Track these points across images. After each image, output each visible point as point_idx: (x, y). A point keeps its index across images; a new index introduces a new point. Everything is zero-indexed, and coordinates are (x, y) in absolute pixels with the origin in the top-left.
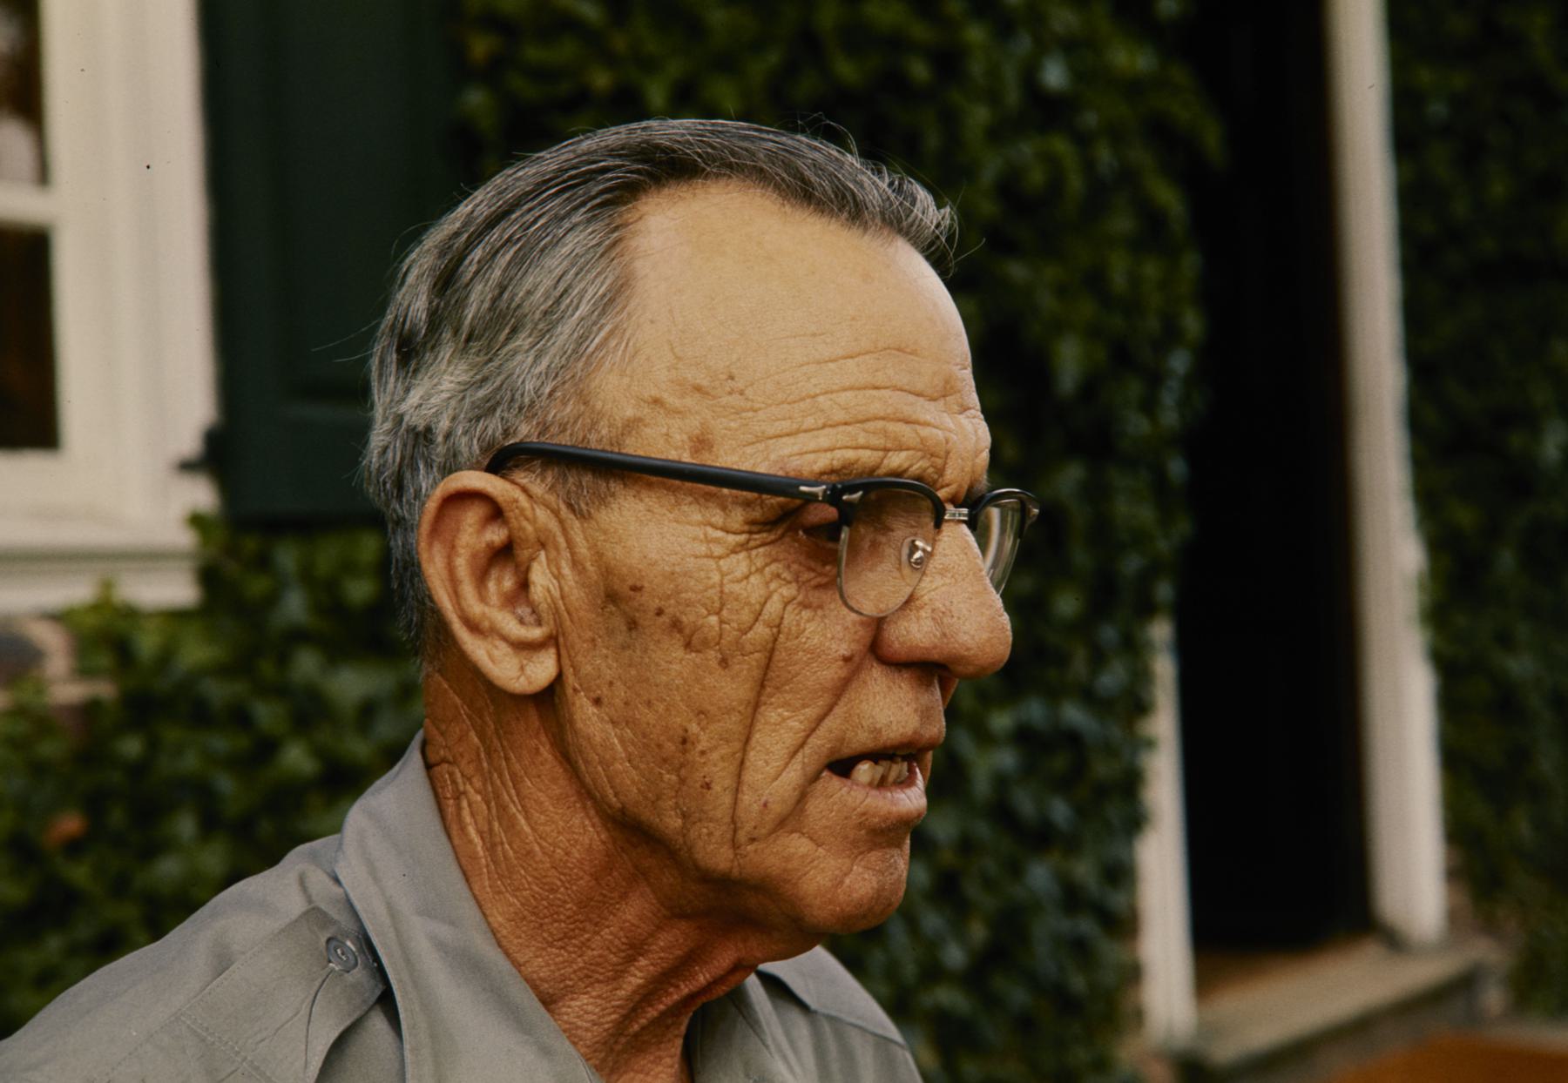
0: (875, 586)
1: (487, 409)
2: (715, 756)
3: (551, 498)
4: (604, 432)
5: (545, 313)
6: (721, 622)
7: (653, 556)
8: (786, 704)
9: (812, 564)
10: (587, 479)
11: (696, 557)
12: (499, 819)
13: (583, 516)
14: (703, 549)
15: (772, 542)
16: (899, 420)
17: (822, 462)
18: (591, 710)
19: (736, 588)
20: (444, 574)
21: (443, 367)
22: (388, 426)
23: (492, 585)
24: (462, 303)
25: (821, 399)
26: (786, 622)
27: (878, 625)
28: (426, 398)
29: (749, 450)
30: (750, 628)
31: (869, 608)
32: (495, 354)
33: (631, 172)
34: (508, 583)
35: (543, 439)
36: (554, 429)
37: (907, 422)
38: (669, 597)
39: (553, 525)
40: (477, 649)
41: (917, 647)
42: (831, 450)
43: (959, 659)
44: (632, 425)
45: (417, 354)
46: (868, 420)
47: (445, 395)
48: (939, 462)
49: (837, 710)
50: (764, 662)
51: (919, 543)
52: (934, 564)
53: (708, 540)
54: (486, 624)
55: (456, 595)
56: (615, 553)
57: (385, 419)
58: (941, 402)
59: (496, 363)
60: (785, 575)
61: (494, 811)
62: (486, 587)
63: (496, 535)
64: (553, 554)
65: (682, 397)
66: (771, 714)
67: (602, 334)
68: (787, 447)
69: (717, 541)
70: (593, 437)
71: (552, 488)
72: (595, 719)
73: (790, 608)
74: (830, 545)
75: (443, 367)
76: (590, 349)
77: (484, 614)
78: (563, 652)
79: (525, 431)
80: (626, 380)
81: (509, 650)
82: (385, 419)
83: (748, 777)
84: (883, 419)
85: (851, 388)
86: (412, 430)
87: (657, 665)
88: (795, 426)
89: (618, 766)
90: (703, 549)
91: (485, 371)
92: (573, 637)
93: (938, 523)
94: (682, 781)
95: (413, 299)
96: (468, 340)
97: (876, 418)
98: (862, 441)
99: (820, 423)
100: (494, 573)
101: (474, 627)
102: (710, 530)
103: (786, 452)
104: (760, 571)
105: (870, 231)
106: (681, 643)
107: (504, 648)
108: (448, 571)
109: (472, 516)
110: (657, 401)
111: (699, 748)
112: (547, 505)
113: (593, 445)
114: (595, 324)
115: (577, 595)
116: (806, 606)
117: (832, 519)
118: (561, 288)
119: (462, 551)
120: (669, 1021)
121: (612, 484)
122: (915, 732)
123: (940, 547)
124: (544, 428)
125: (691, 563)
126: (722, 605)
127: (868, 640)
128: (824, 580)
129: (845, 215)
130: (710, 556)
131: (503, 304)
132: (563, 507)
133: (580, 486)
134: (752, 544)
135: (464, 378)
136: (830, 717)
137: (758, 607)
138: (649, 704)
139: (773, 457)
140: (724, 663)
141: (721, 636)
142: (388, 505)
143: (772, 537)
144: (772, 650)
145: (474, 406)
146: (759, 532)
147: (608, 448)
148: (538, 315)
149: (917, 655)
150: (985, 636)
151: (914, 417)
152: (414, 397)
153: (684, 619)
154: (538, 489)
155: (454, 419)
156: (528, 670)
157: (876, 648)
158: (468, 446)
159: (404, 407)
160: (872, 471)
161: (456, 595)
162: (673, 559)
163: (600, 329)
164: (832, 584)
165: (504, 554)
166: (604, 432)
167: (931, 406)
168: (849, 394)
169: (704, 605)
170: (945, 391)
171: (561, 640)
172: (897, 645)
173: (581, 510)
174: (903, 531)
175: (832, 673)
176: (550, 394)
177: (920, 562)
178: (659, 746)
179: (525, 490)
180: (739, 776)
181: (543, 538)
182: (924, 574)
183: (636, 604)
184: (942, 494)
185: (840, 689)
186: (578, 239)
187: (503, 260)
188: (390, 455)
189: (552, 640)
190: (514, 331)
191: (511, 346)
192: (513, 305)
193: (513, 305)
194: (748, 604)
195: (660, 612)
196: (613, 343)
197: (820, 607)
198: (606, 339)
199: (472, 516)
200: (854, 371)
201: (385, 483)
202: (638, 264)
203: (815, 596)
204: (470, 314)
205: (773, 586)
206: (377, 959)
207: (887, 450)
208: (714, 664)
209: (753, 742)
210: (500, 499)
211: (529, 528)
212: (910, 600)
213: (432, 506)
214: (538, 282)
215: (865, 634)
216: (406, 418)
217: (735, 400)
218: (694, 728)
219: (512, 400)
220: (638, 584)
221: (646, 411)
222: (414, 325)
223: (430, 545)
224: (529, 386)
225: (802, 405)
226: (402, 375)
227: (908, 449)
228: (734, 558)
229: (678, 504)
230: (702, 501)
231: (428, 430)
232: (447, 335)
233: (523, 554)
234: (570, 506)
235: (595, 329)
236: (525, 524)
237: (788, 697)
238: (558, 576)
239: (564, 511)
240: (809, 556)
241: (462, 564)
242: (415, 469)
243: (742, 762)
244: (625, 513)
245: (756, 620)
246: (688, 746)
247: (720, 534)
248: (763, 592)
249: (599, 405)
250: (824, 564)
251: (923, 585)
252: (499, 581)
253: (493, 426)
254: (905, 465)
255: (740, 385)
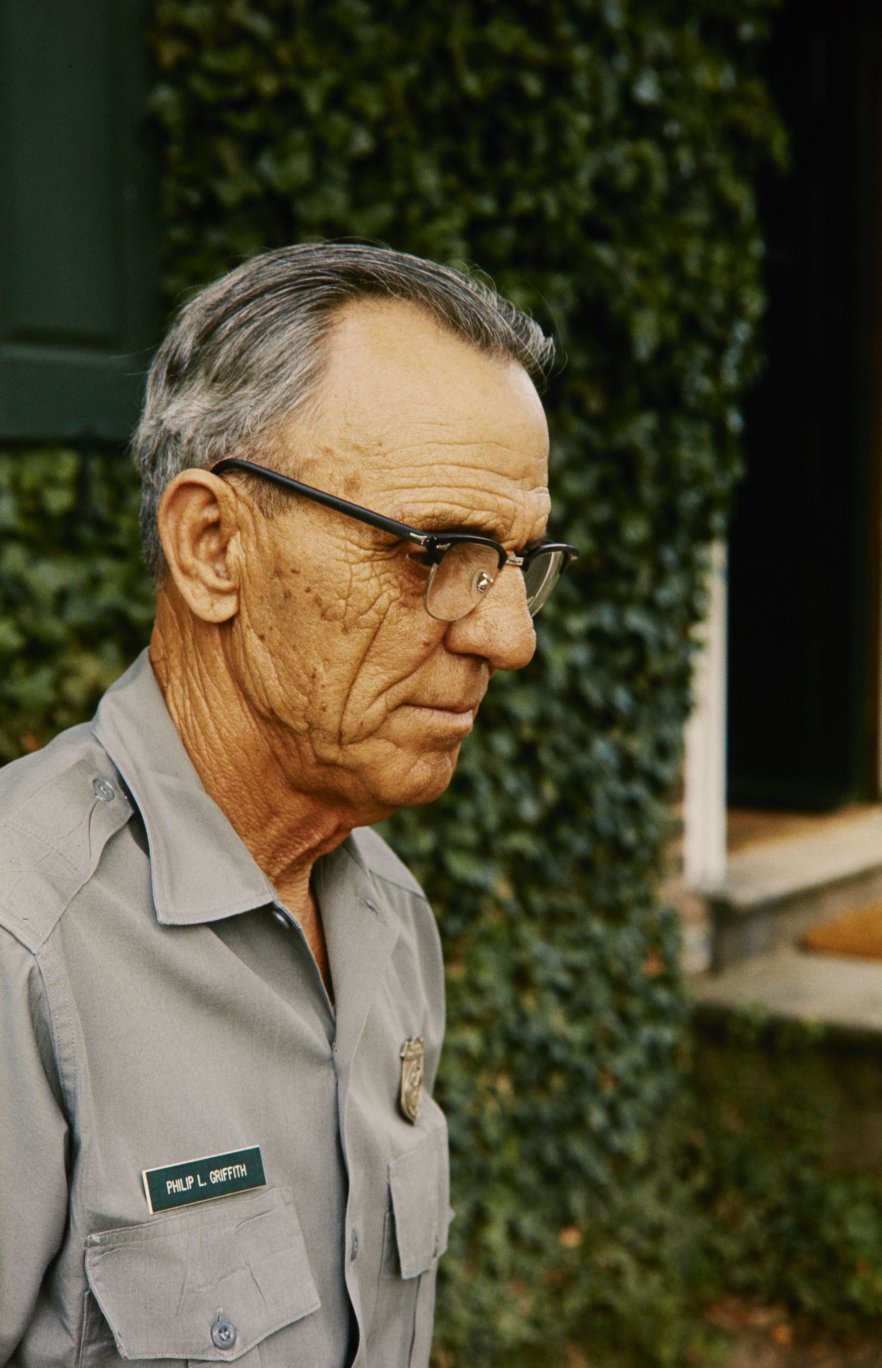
0: (451, 596)
1: (219, 430)
2: (331, 689)
3: (250, 499)
4: (291, 464)
5: (267, 376)
6: (347, 605)
7: (309, 553)
8: (381, 665)
9: (412, 578)
10: (275, 493)
11: (337, 560)
12: (190, 698)
13: (269, 517)
14: (343, 555)
15: (390, 559)
16: (486, 490)
17: (427, 510)
18: (257, 641)
19: (360, 585)
20: (173, 533)
21: (195, 394)
22: (153, 422)
23: (203, 546)
24: (214, 355)
25: (436, 467)
26: (389, 613)
27: (449, 626)
28: (180, 412)
29: (382, 494)
30: (366, 612)
31: (444, 615)
32: (230, 395)
33: (344, 288)
34: (214, 545)
35: (250, 460)
36: (259, 455)
37: (490, 492)
38: (316, 582)
39: (248, 517)
40: (185, 586)
41: (471, 644)
42: (435, 502)
43: (498, 658)
44: (309, 464)
45: (179, 380)
46: (464, 487)
47: (193, 414)
48: (508, 522)
49: (415, 675)
50: (371, 634)
51: (485, 575)
52: (492, 592)
53: (347, 551)
54: (194, 572)
55: (178, 548)
56: (286, 547)
57: (151, 418)
58: (519, 483)
59: (229, 401)
60: (394, 582)
61: (187, 693)
62: (198, 545)
63: (211, 514)
64: (245, 535)
65: (346, 450)
66: (369, 669)
67: (302, 398)
68: (406, 496)
69: (353, 552)
70: (283, 467)
71: (251, 493)
72: (259, 648)
73: (393, 604)
74: (426, 567)
75: (195, 394)
76: (292, 407)
77: (194, 565)
78: (243, 601)
79: (240, 452)
80: (312, 432)
81: (206, 591)
82: (151, 418)
83: (350, 705)
84: (474, 488)
85: (458, 465)
86: (167, 432)
87: (302, 624)
88: (415, 483)
89: (271, 682)
90: (343, 555)
91: (221, 405)
92: (249, 592)
93: (501, 566)
94: (310, 702)
95: (183, 337)
96: (215, 380)
97: (469, 487)
98: (456, 499)
99: (431, 483)
100: (206, 538)
101: (185, 571)
102: (349, 544)
103: (406, 499)
104: (377, 576)
105: (494, 357)
106: (320, 612)
107: (202, 589)
108: (174, 533)
109: (197, 498)
110: (328, 451)
111: (322, 683)
112: (247, 504)
113: (283, 472)
114: (298, 390)
115: (257, 567)
116: (404, 605)
117: (428, 550)
118: (280, 361)
119: (186, 520)
120: (298, 868)
121: (290, 500)
122: (459, 702)
123: (499, 581)
124: (254, 452)
125: (333, 564)
126: (348, 596)
127: (441, 634)
128: (418, 590)
129: (479, 343)
130: (346, 561)
131: (240, 362)
132: (256, 506)
133: (269, 497)
134: (375, 558)
135: (207, 405)
136: (410, 678)
137: (372, 600)
138: (294, 648)
139: (396, 502)
140: (345, 630)
141: (345, 613)
142: (144, 472)
143: (389, 555)
144: (379, 629)
145: (210, 426)
146: (381, 551)
147: (292, 477)
148: (262, 376)
149: (470, 649)
150: (516, 645)
151: (496, 490)
152: (172, 410)
153: (323, 598)
154: (243, 491)
155: (196, 430)
156: (216, 607)
157: (445, 639)
158: (202, 453)
159: (164, 415)
160: (461, 521)
161: (178, 548)
162: (322, 558)
163: (301, 394)
164: (421, 593)
165: (214, 526)
166: (291, 464)
167: (511, 484)
168: (455, 469)
169: (338, 593)
170: (523, 475)
171: (242, 592)
172: (458, 641)
173: (267, 513)
174: (480, 566)
175: (416, 651)
176: (261, 431)
177: (484, 588)
178: (298, 676)
179: (234, 490)
180: (345, 704)
181: (240, 524)
182: (485, 597)
183: (293, 582)
184: (505, 545)
185: (421, 662)
186: (296, 330)
187: (246, 332)
188: (151, 442)
189: (235, 591)
190: (245, 382)
191: (241, 392)
192: (247, 365)
193: (247, 365)
194: (367, 597)
195: (308, 590)
196: (308, 405)
197: (414, 607)
198: (305, 401)
199: (197, 498)
200: (464, 454)
201: (144, 460)
202: (334, 354)
203: (410, 600)
204: (218, 363)
205: (384, 587)
206: (276, 1333)
207: (473, 509)
208: (339, 630)
209: (356, 684)
210: (217, 493)
211: (232, 515)
212: (472, 612)
213: (171, 487)
214: (266, 353)
215: (440, 631)
216: (165, 423)
217: (379, 460)
218: (321, 669)
219: (236, 429)
220: (297, 569)
221: (320, 456)
222: (180, 359)
223: (167, 512)
224: (248, 423)
225: (422, 469)
226: (167, 391)
227: (487, 510)
228: (362, 565)
229: (331, 521)
230: (346, 523)
231: (178, 434)
232: (201, 373)
233: (226, 530)
234: (261, 508)
235: (297, 394)
236: (230, 512)
237: (384, 660)
238: (246, 551)
239: (256, 509)
240: (412, 572)
241: (185, 529)
242: (165, 456)
243: (348, 696)
244: (296, 520)
245: (370, 608)
246: (316, 680)
247: (355, 548)
248: (377, 591)
249: (291, 446)
250: (420, 580)
251: (482, 604)
252: (208, 543)
253: (221, 442)
254: (484, 521)
255: (383, 449)
